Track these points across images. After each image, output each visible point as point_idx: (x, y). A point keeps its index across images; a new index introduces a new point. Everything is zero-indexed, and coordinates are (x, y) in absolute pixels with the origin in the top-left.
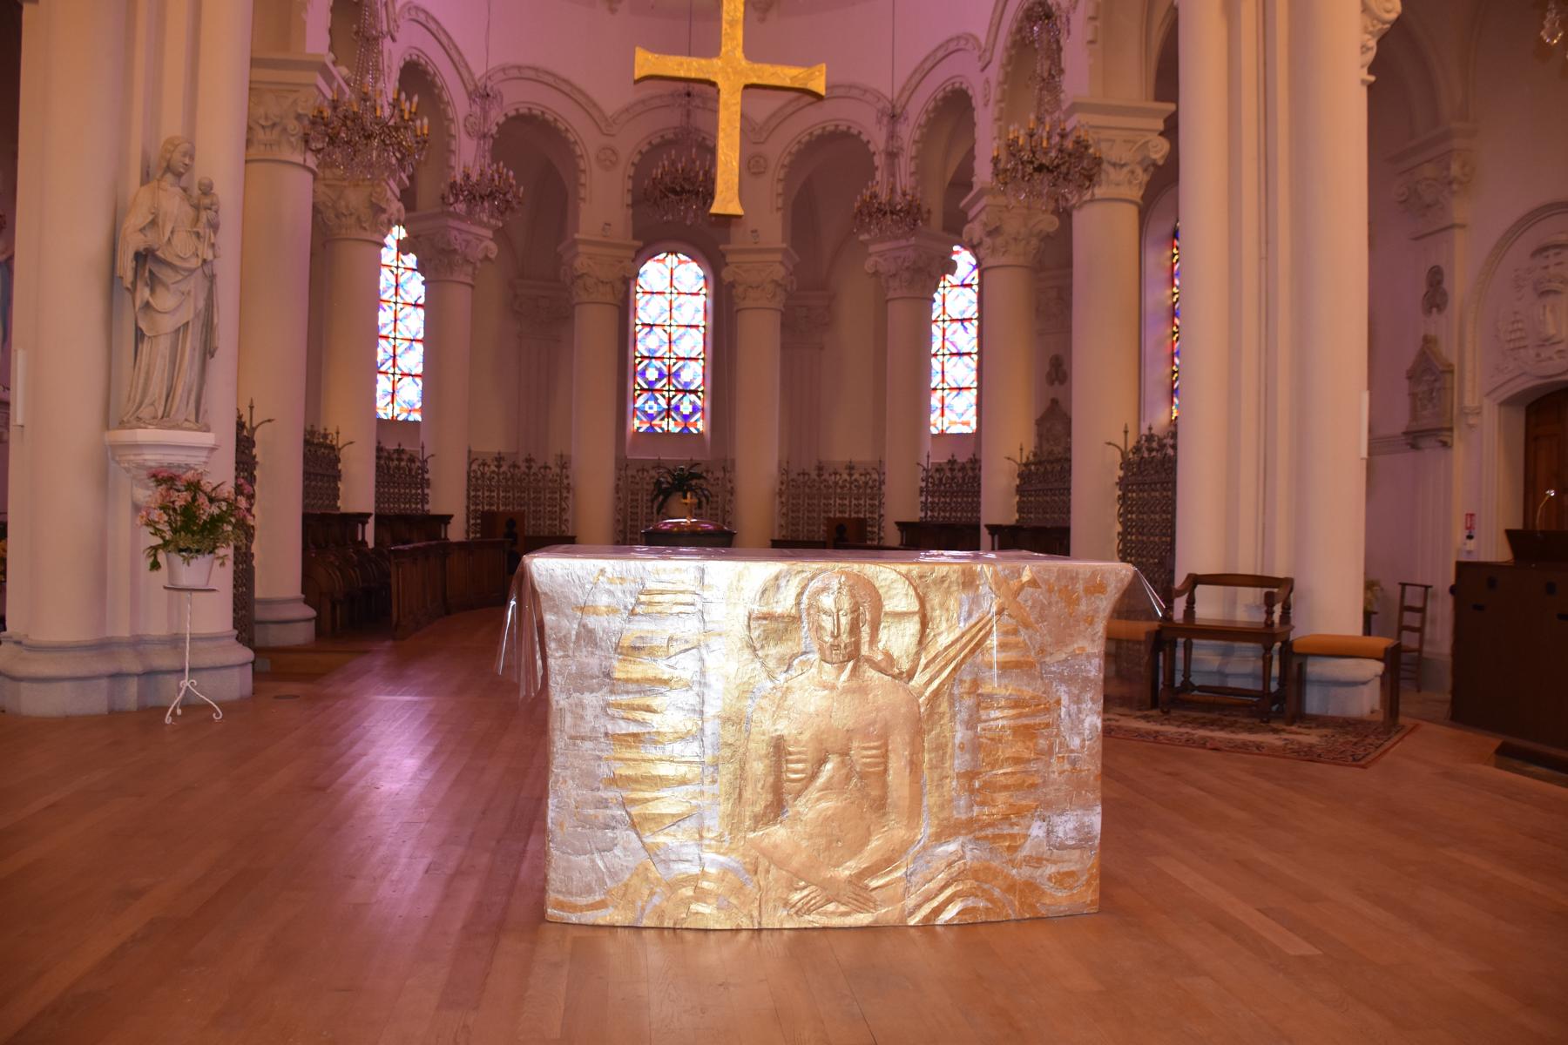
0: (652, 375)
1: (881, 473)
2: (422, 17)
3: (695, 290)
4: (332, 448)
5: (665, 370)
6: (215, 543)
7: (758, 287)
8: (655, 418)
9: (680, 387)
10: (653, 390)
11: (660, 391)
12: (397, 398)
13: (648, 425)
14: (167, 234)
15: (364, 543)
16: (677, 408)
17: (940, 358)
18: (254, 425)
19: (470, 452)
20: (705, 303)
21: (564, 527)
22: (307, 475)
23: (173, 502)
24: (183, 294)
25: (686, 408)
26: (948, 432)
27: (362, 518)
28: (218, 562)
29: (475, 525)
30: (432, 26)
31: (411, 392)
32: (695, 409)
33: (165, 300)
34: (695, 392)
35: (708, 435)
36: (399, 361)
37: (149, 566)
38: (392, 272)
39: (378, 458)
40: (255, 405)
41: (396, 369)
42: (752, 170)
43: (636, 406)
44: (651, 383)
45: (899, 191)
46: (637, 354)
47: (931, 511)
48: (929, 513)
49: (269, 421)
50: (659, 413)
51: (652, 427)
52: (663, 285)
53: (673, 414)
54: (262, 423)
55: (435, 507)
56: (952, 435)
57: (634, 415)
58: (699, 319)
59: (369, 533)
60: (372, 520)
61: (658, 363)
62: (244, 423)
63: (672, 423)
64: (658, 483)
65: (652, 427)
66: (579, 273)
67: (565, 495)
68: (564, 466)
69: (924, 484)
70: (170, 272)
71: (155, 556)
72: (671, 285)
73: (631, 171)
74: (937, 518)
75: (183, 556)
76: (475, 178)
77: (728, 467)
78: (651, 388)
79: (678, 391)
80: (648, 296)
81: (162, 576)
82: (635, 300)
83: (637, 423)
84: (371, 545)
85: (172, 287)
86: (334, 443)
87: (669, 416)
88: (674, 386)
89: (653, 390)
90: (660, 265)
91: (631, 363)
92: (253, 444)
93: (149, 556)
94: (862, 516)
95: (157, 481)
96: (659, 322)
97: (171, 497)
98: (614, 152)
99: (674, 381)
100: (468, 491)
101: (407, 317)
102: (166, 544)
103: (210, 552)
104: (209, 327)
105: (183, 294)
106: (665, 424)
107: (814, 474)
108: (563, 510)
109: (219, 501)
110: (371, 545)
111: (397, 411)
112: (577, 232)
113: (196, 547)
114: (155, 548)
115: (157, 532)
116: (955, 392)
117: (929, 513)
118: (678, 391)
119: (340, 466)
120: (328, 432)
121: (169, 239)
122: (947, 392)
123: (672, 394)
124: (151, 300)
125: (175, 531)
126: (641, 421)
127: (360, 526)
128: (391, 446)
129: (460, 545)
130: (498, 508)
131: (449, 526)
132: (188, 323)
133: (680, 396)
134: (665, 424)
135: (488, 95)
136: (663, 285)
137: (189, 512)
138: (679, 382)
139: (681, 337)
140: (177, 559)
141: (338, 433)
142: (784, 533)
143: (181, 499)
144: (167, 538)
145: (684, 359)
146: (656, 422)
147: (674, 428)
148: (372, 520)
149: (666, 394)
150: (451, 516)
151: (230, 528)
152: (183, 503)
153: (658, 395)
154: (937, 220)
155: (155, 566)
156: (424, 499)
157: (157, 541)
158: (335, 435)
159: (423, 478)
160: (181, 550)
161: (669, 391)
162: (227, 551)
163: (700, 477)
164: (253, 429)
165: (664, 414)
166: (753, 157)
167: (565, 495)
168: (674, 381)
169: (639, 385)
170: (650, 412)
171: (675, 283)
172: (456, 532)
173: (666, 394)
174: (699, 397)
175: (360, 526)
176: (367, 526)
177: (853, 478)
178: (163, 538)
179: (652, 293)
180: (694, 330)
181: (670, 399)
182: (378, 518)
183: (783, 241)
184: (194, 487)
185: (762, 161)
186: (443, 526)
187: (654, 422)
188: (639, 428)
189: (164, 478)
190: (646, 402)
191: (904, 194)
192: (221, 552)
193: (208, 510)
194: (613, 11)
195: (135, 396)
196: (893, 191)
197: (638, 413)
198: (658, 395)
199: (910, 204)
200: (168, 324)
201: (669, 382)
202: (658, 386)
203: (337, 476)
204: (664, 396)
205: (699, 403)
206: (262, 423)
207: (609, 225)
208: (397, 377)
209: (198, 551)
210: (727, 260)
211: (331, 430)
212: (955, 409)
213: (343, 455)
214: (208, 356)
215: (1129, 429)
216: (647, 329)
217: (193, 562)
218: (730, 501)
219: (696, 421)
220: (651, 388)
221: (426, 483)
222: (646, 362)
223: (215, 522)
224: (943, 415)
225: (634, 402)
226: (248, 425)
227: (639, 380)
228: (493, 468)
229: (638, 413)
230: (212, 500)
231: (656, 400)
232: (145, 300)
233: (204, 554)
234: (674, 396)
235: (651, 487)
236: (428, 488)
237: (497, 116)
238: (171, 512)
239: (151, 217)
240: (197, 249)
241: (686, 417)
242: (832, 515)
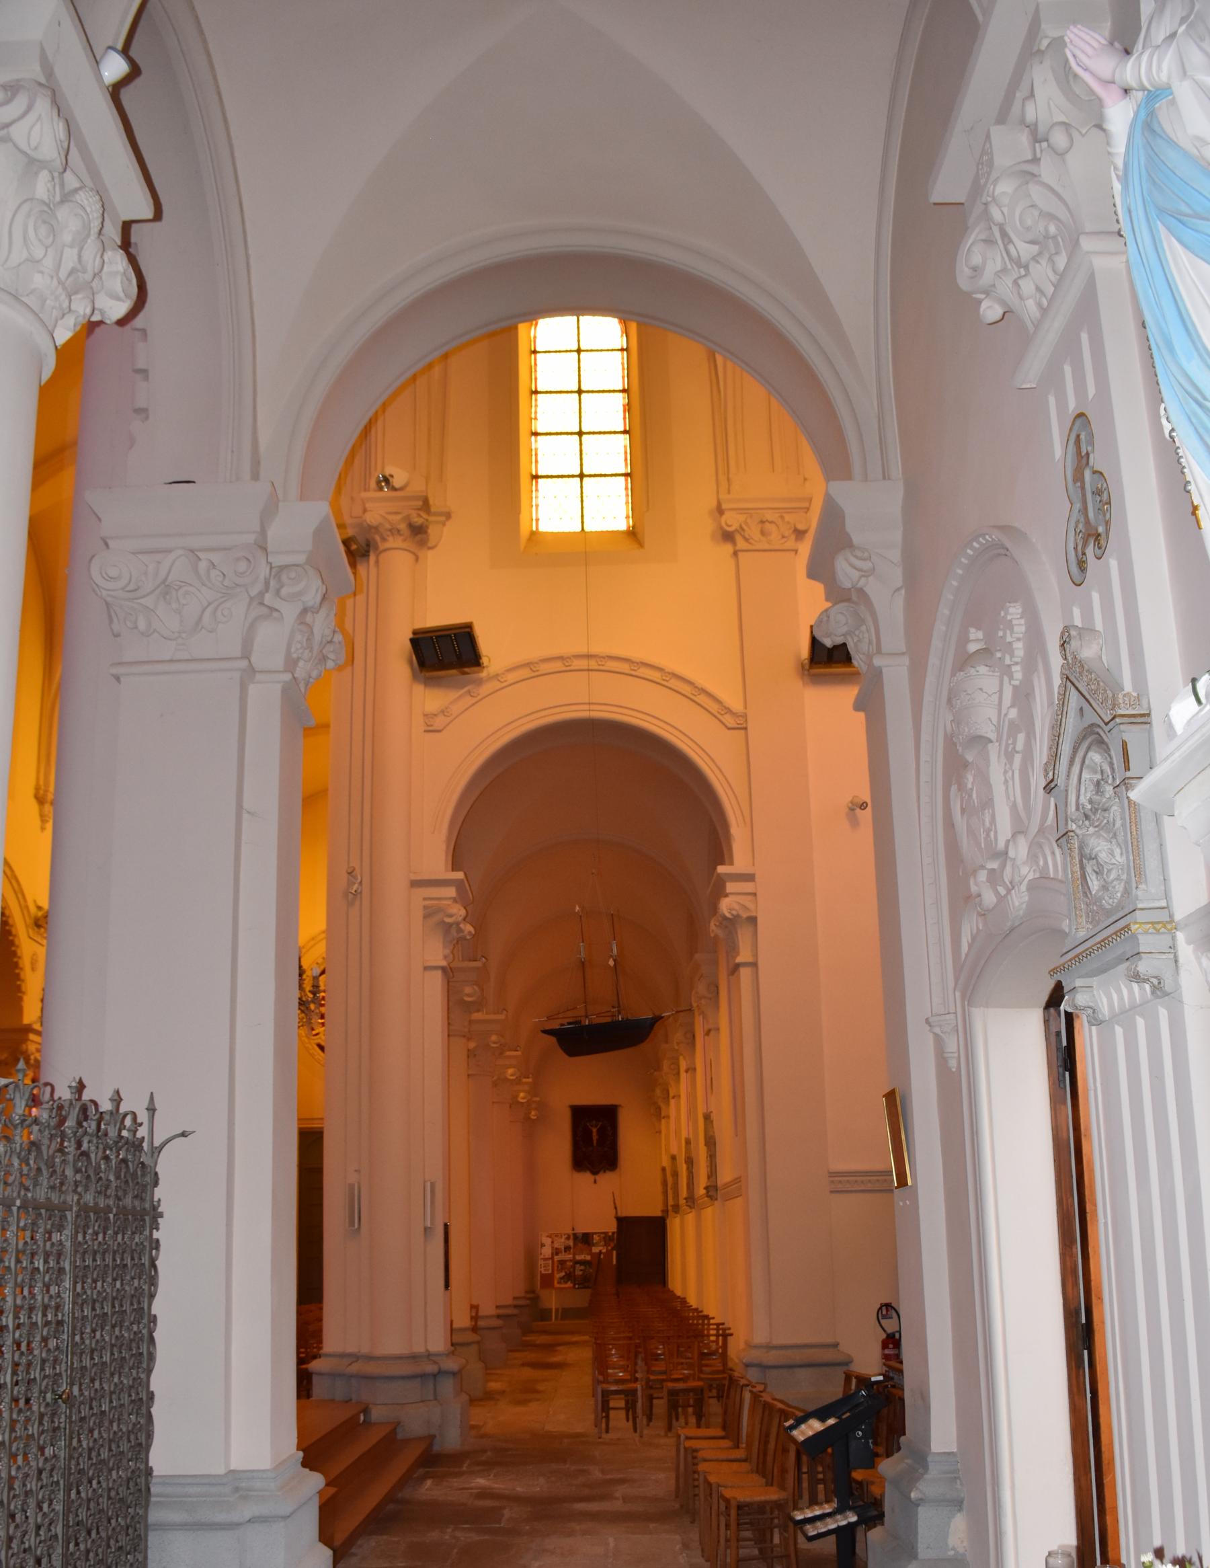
18: (157, 1143)
49: (184, 1134)
141: (152, 1110)
213: (165, 1166)
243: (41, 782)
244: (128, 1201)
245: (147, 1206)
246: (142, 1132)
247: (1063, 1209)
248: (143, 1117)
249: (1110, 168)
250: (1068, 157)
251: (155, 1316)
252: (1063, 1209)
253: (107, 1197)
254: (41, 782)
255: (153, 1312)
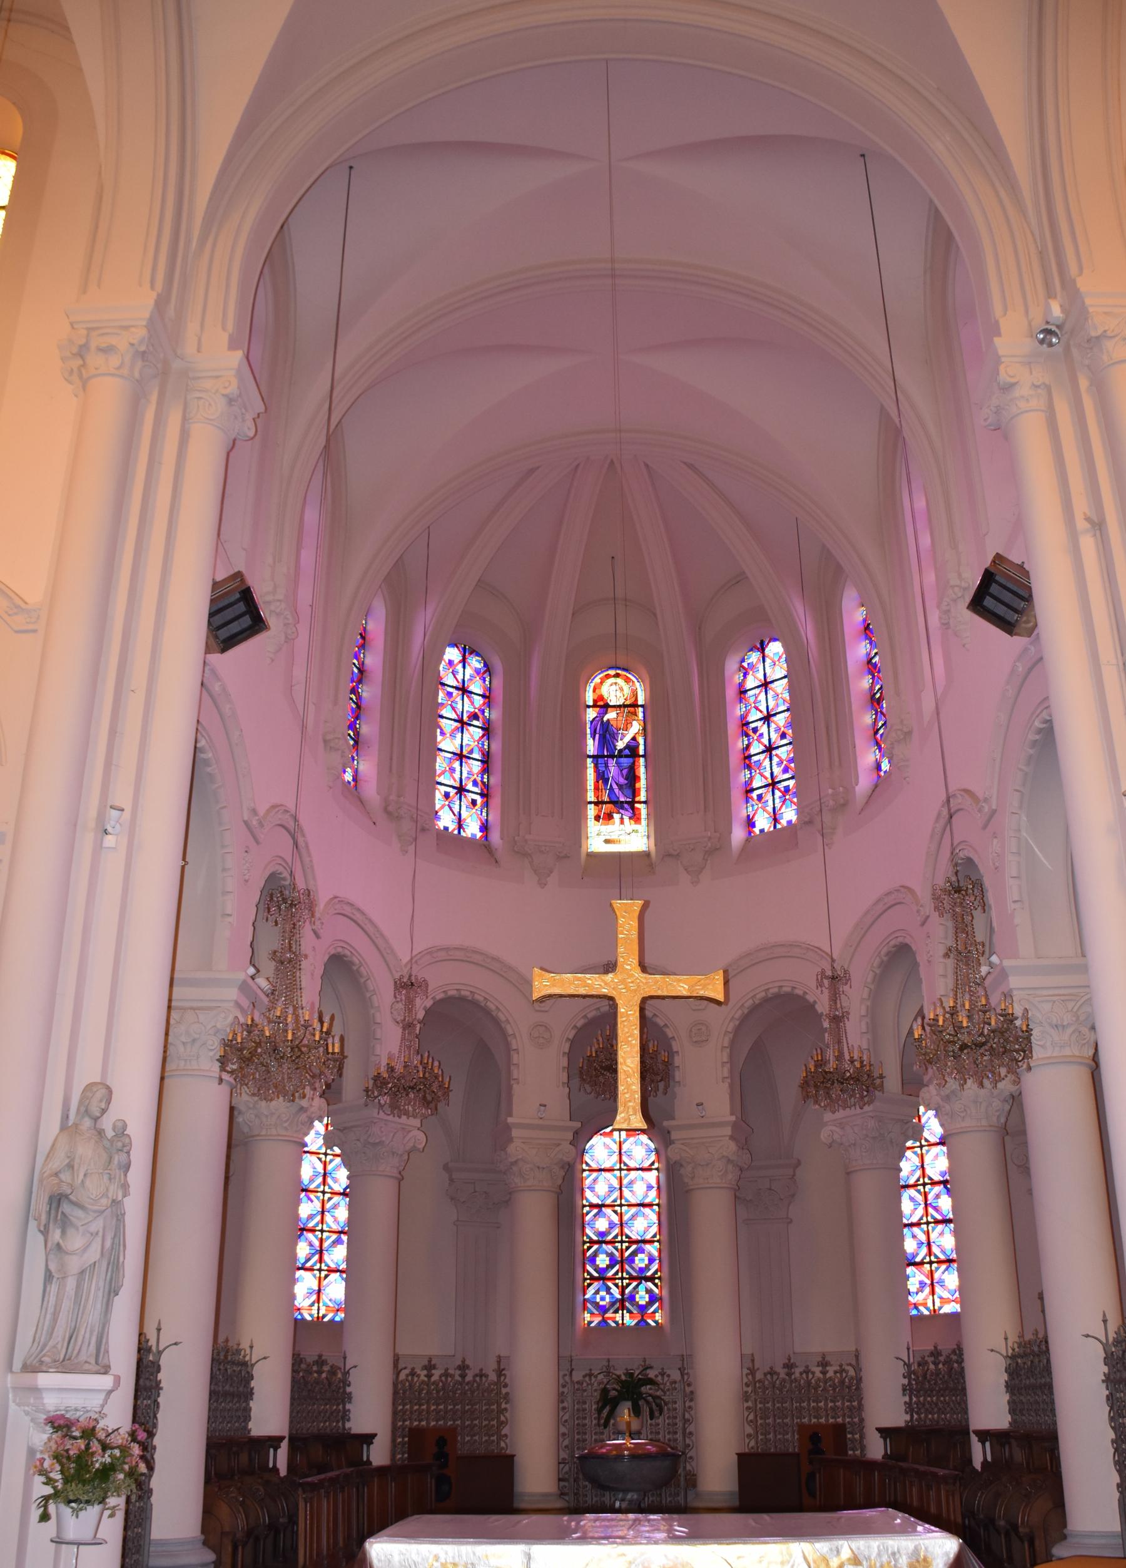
0: (602, 1261)
1: (858, 1369)
2: (347, 910)
3: (646, 1164)
4: (245, 1364)
5: (617, 1254)
6: (106, 1493)
7: (707, 1165)
8: (608, 1310)
9: (634, 1274)
10: (605, 1279)
11: (612, 1279)
12: (323, 1297)
13: (600, 1319)
14: (81, 1177)
15: (275, 1470)
16: (632, 1298)
17: (924, 1227)
18: (161, 1348)
19: (396, 1360)
20: (658, 1177)
21: (503, 1444)
22: (214, 1395)
23: (67, 1451)
24: (92, 1234)
25: (642, 1298)
26: (942, 1312)
27: (274, 1442)
28: (107, 1513)
29: (403, 1444)
30: (358, 917)
31: (336, 1289)
32: (653, 1299)
33: (75, 1241)
34: (651, 1279)
35: (667, 1328)
36: (326, 1257)
37: (37, 1519)
38: (320, 1159)
39: (295, 1371)
40: (162, 1326)
41: (323, 1265)
42: (694, 1039)
43: (587, 1297)
44: (602, 1271)
45: (847, 1057)
46: (585, 1202)
47: (917, 1413)
48: (915, 1416)
49: (176, 1344)
50: (612, 1304)
51: (604, 1321)
52: (612, 1161)
53: (627, 1304)
54: (170, 1345)
55: (359, 1424)
56: (946, 1315)
57: (585, 1308)
58: (652, 1197)
59: (281, 1459)
60: (285, 1445)
61: (609, 1248)
62: (151, 1347)
63: (627, 1315)
64: (605, 1391)
65: (604, 1321)
66: (514, 1160)
67: (503, 1406)
68: (500, 1372)
69: (906, 1381)
70: (80, 1213)
71: (46, 1507)
72: (621, 1161)
73: (566, 1047)
74: (938, 1422)
75: (72, 1508)
76: (399, 1068)
77: (686, 1364)
78: (602, 1276)
79: (632, 1278)
80: (595, 1174)
81: (50, 1526)
82: (582, 1180)
83: (587, 1317)
84: (283, 1472)
85: (81, 1229)
86: (247, 1358)
87: (623, 1307)
88: (628, 1273)
89: (605, 1279)
90: (607, 1140)
91: (579, 1250)
92: (159, 1370)
93: (39, 1507)
94: (840, 1420)
95: (54, 1428)
96: (608, 1202)
97: (65, 1446)
98: (547, 1028)
99: (627, 1267)
100: (394, 1404)
101: (335, 1206)
102: (56, 1495)
103: (100, 1503)
104: (115, 1266)
105: (92, 1234)
106: (618, 1317)
107: (783, 1373)
108: (502, 1424)
109: (112, 1448)
110: (283, 1472)
111: (322, 1312)
112: (510, 1115)
113: (86, 1498)
114: (46, 1498)
115: (49, 1481)
116: (944, 1267)
117: (915, 1416)
118: (632, 1278)
119: (253, 1384)
120: (241, 1347)
121: (82, 1181)
122: (935, 1266)
123: (626, 1282)
124: (61, 1242)
125: (67, 1481)
126: (592, 1314)
127: (272, 1450)
128: (310, 1355)
129: (381, 1470)
130: (428, 1423)
131: (371, 1446)
132: (95, 1262)
133: (634, 1284)
134: (618, 1317)
135: (412, 984)
136: (612, 1161)
137: (82, 1460)
138: (633, 1268)
139: (633, 1217)
140: (66, 1511)
141: (251, 1347)
142: (752, 1443)
143: (75, 1447)
144: (60, 1487)
145: (637, 1242)
146: (609, 1315)
147: (629, 1321)
148: (285, 1445)
149: (619, 1282)
150: (374, 1436)
151: (121, 1476)
152: (77, 1452)
153: (610, 1284)
154: (892, 1083)
155: (45, 1517)
156: (345, 1416)
157: (49, 1490)
158: (248, 1351)
159: (344, 1391)
160: (70, 1501)
161: (622, 1278)
162: (116, 1501)
163: (651, 1382)
164: (160, 1353)
165: (618, 1305)
166: (691, 1031)
167: (503, 1406)
168: (627, 1267)
169: (589, 1273)
170: (602, 1303)
171: (624, 1158)
172: (379, 1455)
173: (619, 1282)
174: (656, 1285)
175: (272, 1450)
176: (279, 1451)
177: (828, 1375)
178: (54, 1488)
179: (600, 1170)
180: (647, 1210)
181: (623, 1288)
182: (292, 1439)
183: (732, 1114)
184: (89, 1433)
185: (704, 1028)
186: (365, 1446)
187: (607, 1315)
188: (590, 1322)
189: (60, 1425)
190: (597, 1292)
191: (852, 1061)
192: (112, 1501)
193: (101, 1460)
194: (542, 884)
195: (40, 1338)
196: (839, 1057)
197: (589, 1305)
198: (610, 1284)
199: (859, 1071)
200: (74, 1264)
201: (622, 1270)
202: (610, 1274)
203: (249, 1394)
204: (616, 1285)
205: (656, 1291)
206: (170, 1345)
207: (545, 1106)
208: (323, 1274)
209: (88, 1502)
210: (673, 1137)
211: (245, 1345)
212: (946, 1284)
213: (256, 1372)
214: (112, 1294)
215: (1108, 1317)
216: (595, 1211)
217: (82, 1514)
218: (690, 1407)
219: (654, 1312)
220: (602, 1276)
221: (349, 1397)
222: (595, 1247)
223: (106, 1472)
224: (933, 1292)
225: (585, 1294)
226: (154, 1349)
227: (589, 1268)
228: (423, 1378)
229: (589, 1305)
230: (105, 1447)
231: (608, 1290)
232: (56, 1242)
233: (93, 1505)
234: (628, 1285)
235: (597, 1394)
236: (350, 1402)
237: (421, 1005)
238: (64, 1460)
239: (67, 1161)
240: (107, 1190)
241: (643, 1309)
242: (806, 1420)
243: (951, 1498)
244: (241, 1389)
245: (154, 1384)
246: (247, 1358)
247: (1037, 247)
248: (248, 1351)
249: (436, 732)
250: (645, 1189)
251: (155, 1446)
252: (1037, 247)
253: (234, 1387)
254: (951, 1498)
255: (154, 1444)
